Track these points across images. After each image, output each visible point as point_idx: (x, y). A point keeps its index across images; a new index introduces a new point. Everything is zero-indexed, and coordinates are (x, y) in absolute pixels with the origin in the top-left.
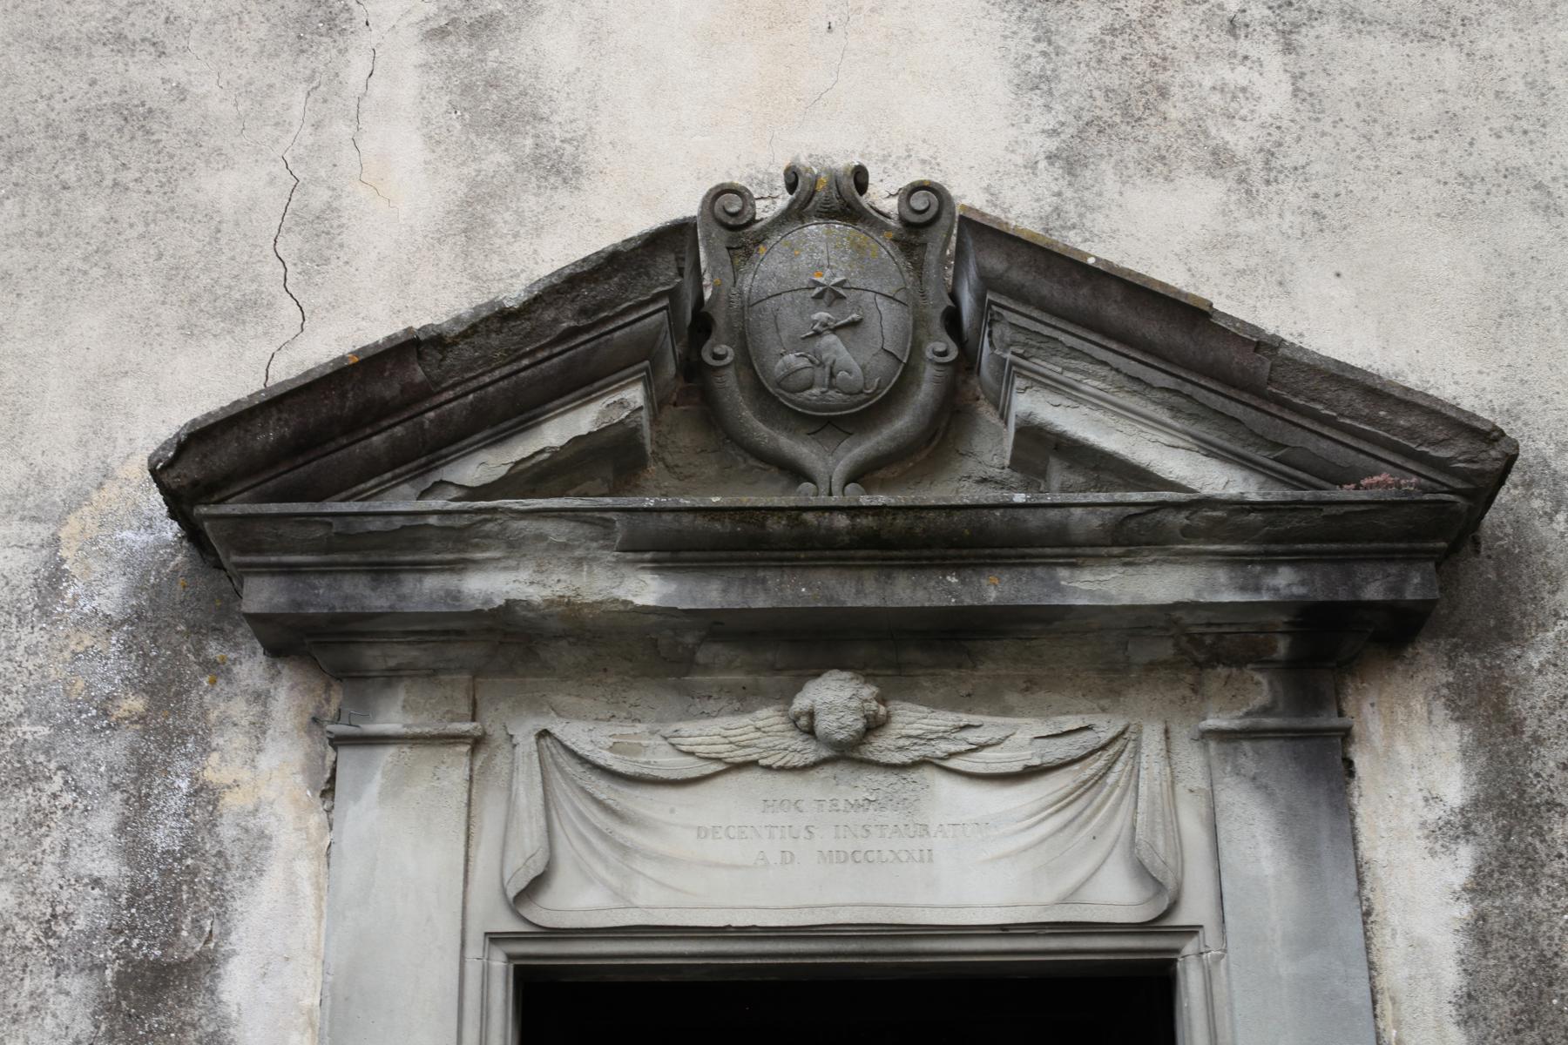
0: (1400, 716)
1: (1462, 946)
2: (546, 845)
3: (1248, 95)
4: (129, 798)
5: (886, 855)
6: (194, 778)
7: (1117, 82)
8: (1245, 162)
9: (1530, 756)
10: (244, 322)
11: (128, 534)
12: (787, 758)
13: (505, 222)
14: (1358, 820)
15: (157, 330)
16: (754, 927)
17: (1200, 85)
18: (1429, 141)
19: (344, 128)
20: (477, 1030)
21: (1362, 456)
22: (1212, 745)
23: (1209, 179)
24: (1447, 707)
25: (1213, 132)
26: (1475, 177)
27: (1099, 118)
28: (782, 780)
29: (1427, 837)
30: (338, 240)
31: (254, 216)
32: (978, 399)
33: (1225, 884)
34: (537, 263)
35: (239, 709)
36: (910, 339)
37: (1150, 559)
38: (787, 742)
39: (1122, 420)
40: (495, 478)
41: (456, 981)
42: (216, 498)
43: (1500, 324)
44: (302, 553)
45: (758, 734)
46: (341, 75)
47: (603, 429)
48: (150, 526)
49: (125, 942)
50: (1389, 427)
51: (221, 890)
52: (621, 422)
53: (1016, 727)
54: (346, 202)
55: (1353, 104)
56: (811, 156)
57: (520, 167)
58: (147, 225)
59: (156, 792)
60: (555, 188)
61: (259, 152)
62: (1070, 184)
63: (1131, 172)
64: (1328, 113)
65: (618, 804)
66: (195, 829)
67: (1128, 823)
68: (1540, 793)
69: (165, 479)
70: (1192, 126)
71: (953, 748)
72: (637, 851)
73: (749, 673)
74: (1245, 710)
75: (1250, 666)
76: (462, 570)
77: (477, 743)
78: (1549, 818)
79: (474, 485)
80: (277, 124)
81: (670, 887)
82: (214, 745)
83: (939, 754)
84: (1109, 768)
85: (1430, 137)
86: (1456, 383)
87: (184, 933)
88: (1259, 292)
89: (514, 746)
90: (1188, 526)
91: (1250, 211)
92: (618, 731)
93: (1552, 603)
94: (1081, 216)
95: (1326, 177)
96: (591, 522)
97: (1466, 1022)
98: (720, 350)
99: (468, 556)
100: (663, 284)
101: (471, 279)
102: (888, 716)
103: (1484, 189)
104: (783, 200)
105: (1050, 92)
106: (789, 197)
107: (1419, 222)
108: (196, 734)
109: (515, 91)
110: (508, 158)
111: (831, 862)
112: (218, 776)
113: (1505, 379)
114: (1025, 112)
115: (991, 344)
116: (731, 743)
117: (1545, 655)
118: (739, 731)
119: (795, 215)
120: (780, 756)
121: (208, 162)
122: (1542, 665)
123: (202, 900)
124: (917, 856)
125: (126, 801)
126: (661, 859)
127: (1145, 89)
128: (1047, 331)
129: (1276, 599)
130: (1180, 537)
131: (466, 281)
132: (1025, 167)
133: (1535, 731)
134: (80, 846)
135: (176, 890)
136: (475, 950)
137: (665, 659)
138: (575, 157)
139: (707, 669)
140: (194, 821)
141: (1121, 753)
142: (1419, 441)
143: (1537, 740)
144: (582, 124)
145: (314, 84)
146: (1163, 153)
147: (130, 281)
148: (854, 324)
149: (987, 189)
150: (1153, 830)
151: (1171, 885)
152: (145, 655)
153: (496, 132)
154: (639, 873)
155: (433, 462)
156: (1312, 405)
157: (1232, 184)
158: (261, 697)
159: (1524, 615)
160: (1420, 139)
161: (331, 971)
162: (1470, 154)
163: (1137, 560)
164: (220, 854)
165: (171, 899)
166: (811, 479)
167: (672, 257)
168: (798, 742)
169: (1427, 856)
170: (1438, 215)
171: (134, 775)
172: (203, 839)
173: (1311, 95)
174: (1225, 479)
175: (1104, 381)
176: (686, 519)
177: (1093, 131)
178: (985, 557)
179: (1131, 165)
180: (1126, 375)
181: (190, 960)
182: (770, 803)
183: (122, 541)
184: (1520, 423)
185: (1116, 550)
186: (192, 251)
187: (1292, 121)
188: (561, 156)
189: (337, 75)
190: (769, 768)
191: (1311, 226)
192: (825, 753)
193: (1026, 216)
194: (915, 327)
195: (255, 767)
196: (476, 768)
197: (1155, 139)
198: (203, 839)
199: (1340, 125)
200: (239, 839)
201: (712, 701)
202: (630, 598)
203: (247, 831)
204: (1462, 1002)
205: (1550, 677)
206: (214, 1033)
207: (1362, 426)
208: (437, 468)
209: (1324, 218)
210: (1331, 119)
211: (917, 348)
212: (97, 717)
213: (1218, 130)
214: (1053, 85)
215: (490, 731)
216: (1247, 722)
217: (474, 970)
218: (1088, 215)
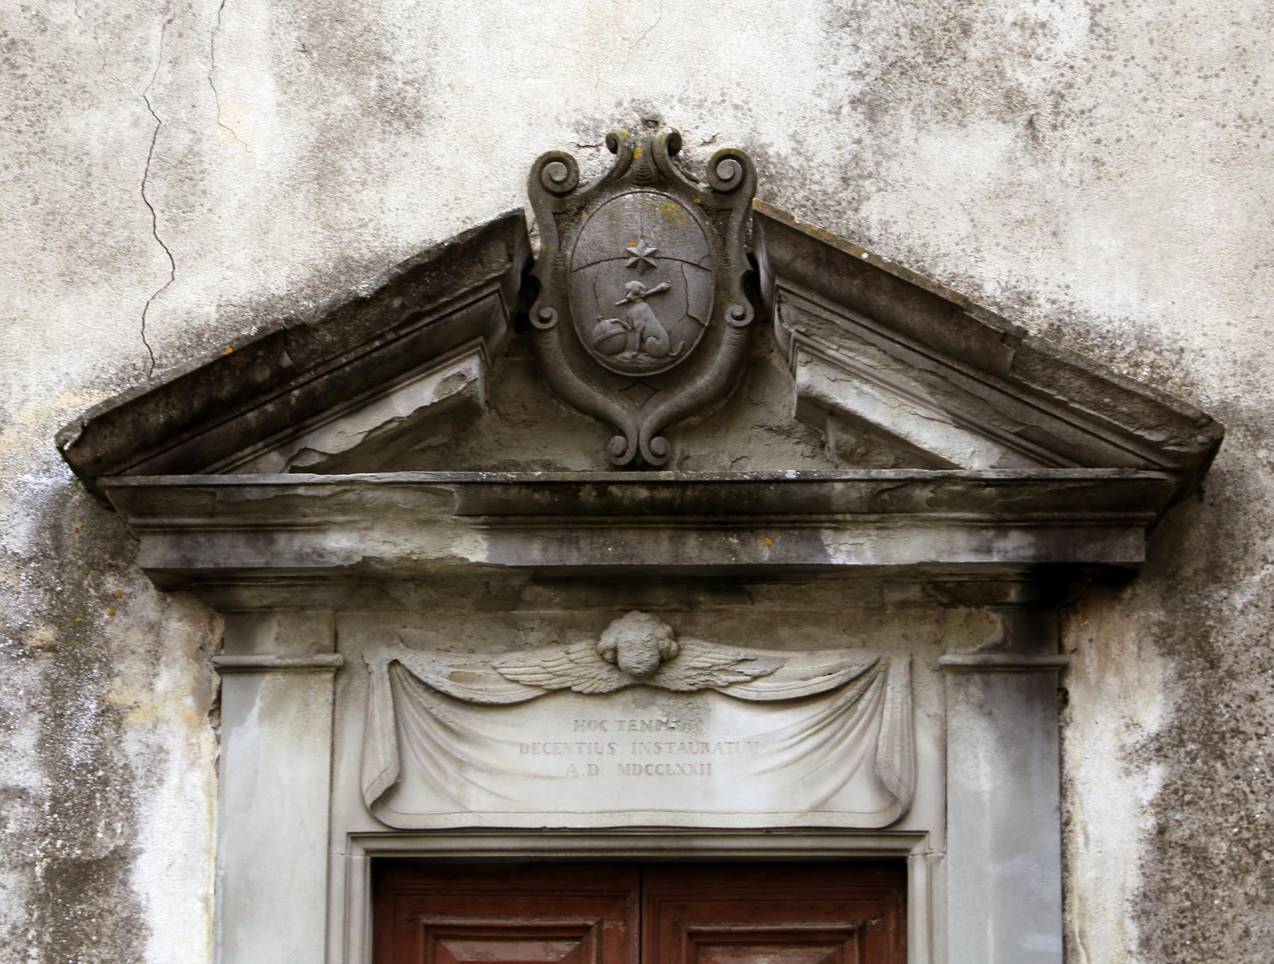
0: (1115, 648)
1: (1143, 853)
2: (396, 759)
3: (1047, 31)
4: (46, 718)
5: (674, 768)
6: (101, 699)
7: (923, 18)
8: (1035, 106)
9: (1223, 688)
10: (119, 270)
11: (28, 477)
12: (595, 686)
13: (354, 169)
14: (1067, 742)
15: (39, 277)
16: (565, 828)
17: (1002, 21)
18: (1214, 80)
19: (201, 66)
20: (342, 914)
21: (1088, 436)
22: (949, 677)
23: (1000, 124)
24: (1156, 642)
25: (1009, 73)
26: (1253, 119)
27: (903, 58)
28: (590, 704)
29: (1124, 759)
30: (201, 186)
31: (121, 160)
32: (772, 351)
33: (949, 797)
34: (383, 212)
35: (137, 639)
36: (712, 303)
37: (899, 524)
38: (594, 671)
39: (887, 393)
40: (352, 445)
41: (323, 874)
42: (116, 470)
43: (1254, 274)
44: (191, 516)
45: (571, 665)
46: (195, 6)
47: (445, 400)
48: (48, 470)
49: (50, 843)
50: (1112, 410)
51: (129, 797)
52: (459, 393)
53: (784, 660)
54: (206, 146)
55: (1147, 40)
56: (633, 100)
57: (366, 112)
58: (21, 167)
59: (69, 712)
60: (398, 134)
61: (122, 90)
62: (870, 131)
63: (927, 117)
64: (1121, 50)
65: (456, 724)
66: (103, 746)
67: (873, 745)
68: (1227, 722)
69: (76, 460)
70: (989, 67)
71: (732, 678)
72: (471, 765)
73: (565, 608)
74: (979, 646)
75: (986, 607)
76: (323, 532)
77: (339, 671)
78: (1232, 744)
79: (334, 452)
80: (136, 60)
81: (498, 795)
82: (116, 670)
83: (719, 683)
84: (861, 696)
85: (1217, 75)
86: (1205, 335)
87: (100, 835)
88: (1033, 243)
89: (370, 673)
90: (932, 498)
91: (1035, 159)
92: (456, 661)
93: (1262, 548)
94: (878, 164)
95: (1110, 121)
96: (435, 492)
97: (1139, 917)
98: (545, 313)
99: (332, 519)
100: (495, 271)
101: (324, 228)
102: (679, 650)
103: (1260, 131)
104: (607, 159)
105: (859, 30)
106: (613, 156)
107: (1192, 168)
108: (101, 661)
109: (359, 27)
110: (354, 100)
111: (628, 774)
112: (121, 698)
113: (1250, 331)
114: (834, 52)
115: (780, 317)
116: (549, 673)
117: (1249, 596)
118: (555, 663)
119: (613, 181)
120: (588, 684)
121: (73, 100)
122: (1245, 606)
123: (113, 806)
124: (698, 769)
125: (43, 721)
126: (491, 771)
127: (948, 26)
128: (825, 315)
129: (1004, 560)
130: (926, 506)
131: (319, 230)
132: (830, 112)
133: (1231, 666)
134: (6, 760)
135: (91, 797)
136: (339, 848)
137: (495, 597)
138: (417, 100)
139: (531, 605)
140: (103, 739)
141: (871, 683)
142: (1137, 426)
143: (1231, 674)
144: (422, 64)
145: (168, 17)
146: (960, 96)
147: (11, 226)
148: (663, 292)
149: (793, 137)
150: (892, 752)
151: (903, 797)
152: (52, 590)
153: (343, 73)
154: (473, 783)
155: (298, 431)
156: (1046, 390)
157: (1020, 129)
158: (153, 628)
159: (1235, 559)
160: (1206, 77)
161: (223, 865)
162: (1253, 94)
163: (889, 525)
164: (126, 766)
165: (87, 805)
166: (622, 433)
167: (502, 246)
168: (604, 672)
169: (1123, 775)
170: (1212, 161)
171: (49, 698)
172: (111, 753)
173: (1107, 30)
174: (972, 449)
175: (873, 359)
176: (513, 492)
177: (896, 72)
178: (762, 522)
179: (928, 110)
180: (891, 356)
181: (106, 858)
182: (580, 723)
183: (24, 483)
184: (1258, 375)
185: (872, 517)
186: (66, 195)
187: (1085, 60)
188: (404, 99)
189: (190, 6)
190: (580, 693)
191: (1090, 173)
192: (626, 682)
193: (828, 165)
194: (717, 290)
195: (151, 690)
196: (339, 692)
197: (952, 82)
198: (111, 753)
199: (1131, 63)
200: (141, 753)
201: (534, 633)
202: (467, 556)
203: (148, 746)
204: (1138, 900)
205: (1251, 617)
206: (128, 918)
207: (1089, 411)
208: (302, 436)
209: (1103, 164)
210: (1124, 57)
211: (717, 313)
212: (13, 646)
213: (1014, 71)
214: (862, 23)
215: (350, 659)
216: (979, 658)
217: (338, 863)
218: (884, 163)
